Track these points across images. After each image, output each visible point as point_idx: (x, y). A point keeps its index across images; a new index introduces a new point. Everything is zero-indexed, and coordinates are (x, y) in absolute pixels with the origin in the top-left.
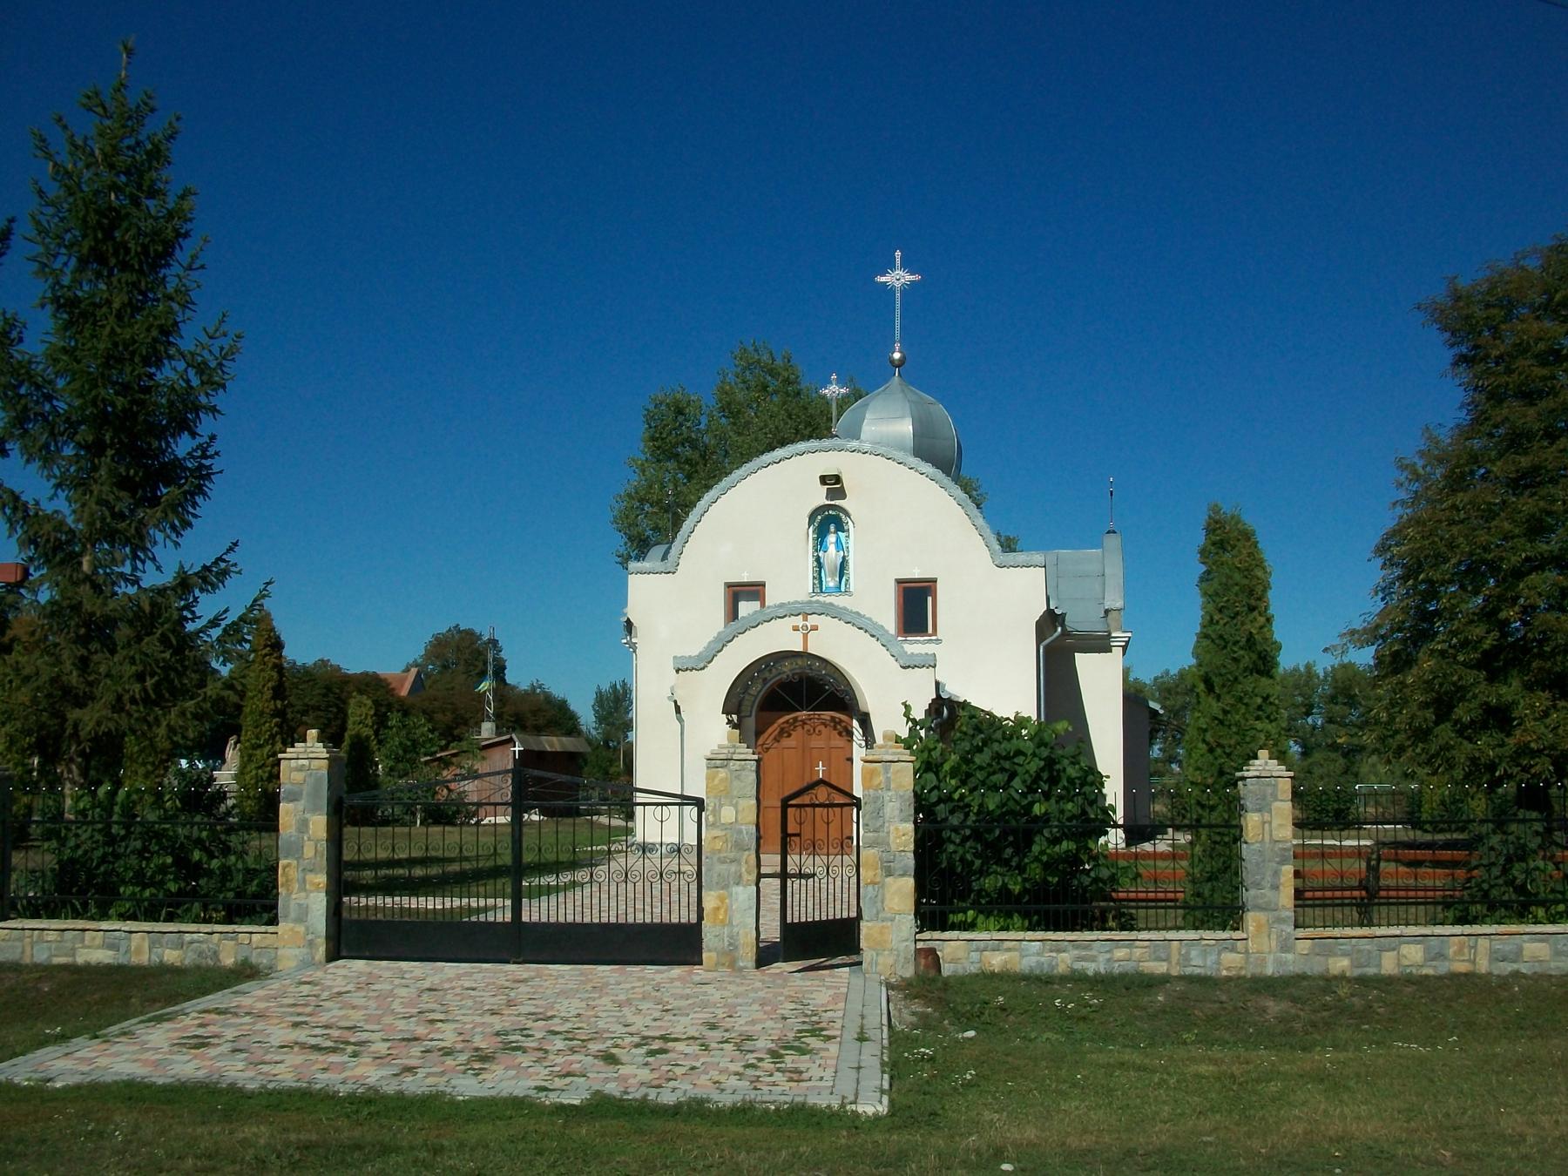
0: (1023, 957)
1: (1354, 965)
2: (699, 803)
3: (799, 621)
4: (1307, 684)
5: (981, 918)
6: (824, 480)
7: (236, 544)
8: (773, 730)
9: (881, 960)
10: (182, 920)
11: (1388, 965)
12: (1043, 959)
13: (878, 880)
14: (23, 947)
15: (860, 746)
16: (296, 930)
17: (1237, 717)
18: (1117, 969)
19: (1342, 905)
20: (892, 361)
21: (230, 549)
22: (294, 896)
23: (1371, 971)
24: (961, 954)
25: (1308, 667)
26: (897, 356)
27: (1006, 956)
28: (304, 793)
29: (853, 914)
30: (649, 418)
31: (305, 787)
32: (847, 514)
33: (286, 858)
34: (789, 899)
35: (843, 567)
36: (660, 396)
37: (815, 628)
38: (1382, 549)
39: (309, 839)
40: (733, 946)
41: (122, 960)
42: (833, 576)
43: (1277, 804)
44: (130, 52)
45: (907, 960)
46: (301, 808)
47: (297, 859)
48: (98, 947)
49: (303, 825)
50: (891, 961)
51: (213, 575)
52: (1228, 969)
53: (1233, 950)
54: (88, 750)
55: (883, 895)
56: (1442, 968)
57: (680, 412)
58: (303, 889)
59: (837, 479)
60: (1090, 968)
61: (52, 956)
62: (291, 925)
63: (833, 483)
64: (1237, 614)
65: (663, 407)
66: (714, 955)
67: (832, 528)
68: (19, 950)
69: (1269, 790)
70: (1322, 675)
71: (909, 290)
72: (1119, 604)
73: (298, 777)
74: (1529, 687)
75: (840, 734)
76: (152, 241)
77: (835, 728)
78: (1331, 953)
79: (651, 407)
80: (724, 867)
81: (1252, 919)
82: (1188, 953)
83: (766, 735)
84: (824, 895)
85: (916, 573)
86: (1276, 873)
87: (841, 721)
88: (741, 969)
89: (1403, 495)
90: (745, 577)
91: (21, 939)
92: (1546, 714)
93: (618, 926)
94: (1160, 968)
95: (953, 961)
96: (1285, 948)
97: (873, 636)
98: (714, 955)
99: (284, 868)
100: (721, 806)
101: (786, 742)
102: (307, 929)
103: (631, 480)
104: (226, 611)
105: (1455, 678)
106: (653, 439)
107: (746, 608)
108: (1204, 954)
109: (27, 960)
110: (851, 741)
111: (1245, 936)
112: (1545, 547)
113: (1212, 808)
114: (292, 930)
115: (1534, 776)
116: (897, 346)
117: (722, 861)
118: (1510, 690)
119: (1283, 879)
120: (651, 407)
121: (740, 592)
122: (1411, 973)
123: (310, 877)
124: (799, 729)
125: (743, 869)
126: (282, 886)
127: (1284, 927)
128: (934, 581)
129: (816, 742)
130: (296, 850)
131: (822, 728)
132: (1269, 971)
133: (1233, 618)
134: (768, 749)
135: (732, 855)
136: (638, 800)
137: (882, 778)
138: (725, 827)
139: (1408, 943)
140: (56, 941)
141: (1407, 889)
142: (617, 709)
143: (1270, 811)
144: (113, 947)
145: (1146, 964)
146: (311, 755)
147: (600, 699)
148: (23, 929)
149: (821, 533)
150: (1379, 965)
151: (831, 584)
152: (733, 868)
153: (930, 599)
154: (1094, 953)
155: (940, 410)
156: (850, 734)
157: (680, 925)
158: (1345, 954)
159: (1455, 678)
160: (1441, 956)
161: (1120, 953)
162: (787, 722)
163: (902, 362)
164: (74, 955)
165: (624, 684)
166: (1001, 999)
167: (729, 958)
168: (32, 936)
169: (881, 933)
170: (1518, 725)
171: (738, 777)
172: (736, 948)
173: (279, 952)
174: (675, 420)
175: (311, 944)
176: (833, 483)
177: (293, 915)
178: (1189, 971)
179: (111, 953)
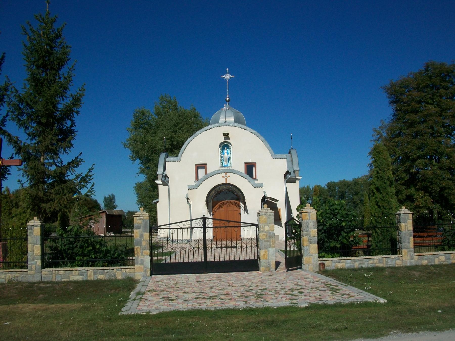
0: (346, 264)
1: (429, 262)
2: (257, 226)
3: (224, 175)
4: (307, 192)
5: (326, 255)
6: (224, 134)
7: (81, 153)
8: (217, 206)
9: (309, 267)
10: (97, 266)
11: (437, 262)
12: (351, 264)
13: (308, 245)
14: (52, 276)
15: (243, 210)
16: (141, 267)
17: (386, 198)
18: (369, 266)
19: (420, 247)
20: (226, 100)
21: (80, 155)
22: (140, 257)
23: (433, 263)
24: (330, 264)
25: (308, 187)
26: (228, 99)
27: (342, 264)
28: (142, 226)
29: (256, 258)
30: (135, 116)
31: (142, 224)
32: (231, 144)
33: (137, 246)
34: (208, 254)
35: (229, 159)
36: (138, 110)
37: (229, 177)
38: (370, 153)
39: (144, 240)
40: (269, 265)
41: (85, 279)
42: (226, 162)
43: (408, 221)
44: (49, 3)
45: (316, 267)
46: (141, 231)
47: (140, 246)
48: (77, 275)
49: (142, 236)
50: (312, 267)
51: (75, 163)
52: (397, 265)
53: (399, 259)
54: (50, 216)
55: (309, 249)
56: (450, 262)
57: (144, 114)
58: (142, 255)
59: (228, 134)
60: (364, 266)
61: (62, 279)
62: (139, 266)
63: (226, 135)
64: (385, 171)
65: (138, 113)
66: (264, 268)
67: (226, 148)
68: (51, 277)
69: (406, 217)
70: (311, 189)
71: (231, 80)
72: (298, 169)
73: (140, 222)
74: (418, 190)
75: (237, 207)
76: (61, 61)
77: (235, 205)
78: (423, 259)
79: (135, 113)
80: (266, 243)
81: (404, 251)
82: (388, 261)
83: (215, 208)
84: (245, 253)
85: (250, 161)
86: (409, 239)
87: (237, 203)
88: (272, 271)
89: (374, 138)
90: (201, 162)
91: (52, 274)
92: (422, 197)
93: (235, 261)
94: (381, 265)
95: (328, 266)
96: (412, 258)
97: (246, 179)
98: (264, 268)
99: (136, 249)
100: (264, 226)
101: (221, 209)
102: (144, 266)
103: (129, 135)
104: (82, 173)
105: (399, 188)
106: (136, 122)
107: (201, 172)
108: (392, 261)
109: (54, 280)
110: (240, 208)
111: (402, 256)
112: (422, 153)
113: (381, 223)
114: (139, 267)
115: (420, 213)
116: (228, 96)
117: (265, 241)
118: (412, 191)
119: (411, 240)
120: (135, 113)
121: (199, 167)
122: (442, 264)
123: (144, 251)
124: (225, 205)
125: (271, 244)
126: (136, 254)
127: (411, 253)
128: (255, 163)
129: (230, 209)
130: (140, 243)
131: (231, 205)
132: (408, 264)
133: (384, 172)
134: (216, 211)
135: (268, 240)
136: (242, 225)
137: (308, 217)
138: (266, 232)
139: (441, 256)
140: (63, 274)
141: (422, 243)
142: (111, 203)
143: (407, 223)
144: (81, 275)
145: (377, 264)
146: (144, 215)
147: (106, 200)
148: (52, 271)
149: (223, 149)
150: (434, 262)
151: (226, 164)
152: (268, 243)
153: (254, 168)
154: (364, 262)
155: (241, 114)
156: (240, 207)
157: (249, 260)
158: (426, 259)
159: (399, 188)
160: (449, 259)
161: (371, 262)
162: (221, 204)
163: (229, 100)
164: (69, 278)
165: (113, 195)
166: (352, 275)
167: (268, 268)
168: (55, 273)
169: (309, 260)
170: (416, 200)
171: (269, 218)
172: (270, 266)
173: (136, 274)
174: (142, 117)
175: (145, 271)
176: (226, 135)
177: (139, 262)
178: (388, 266)
179: (81, 277)
